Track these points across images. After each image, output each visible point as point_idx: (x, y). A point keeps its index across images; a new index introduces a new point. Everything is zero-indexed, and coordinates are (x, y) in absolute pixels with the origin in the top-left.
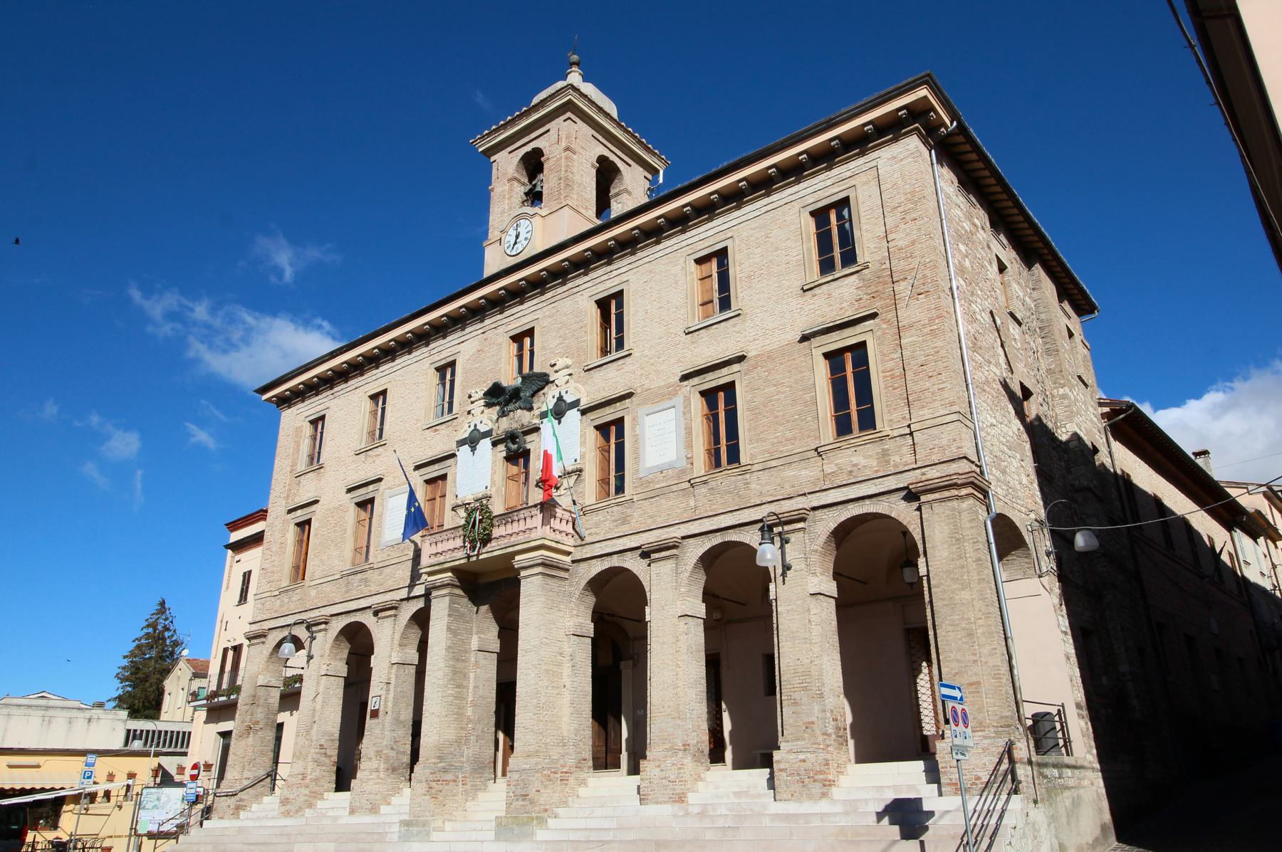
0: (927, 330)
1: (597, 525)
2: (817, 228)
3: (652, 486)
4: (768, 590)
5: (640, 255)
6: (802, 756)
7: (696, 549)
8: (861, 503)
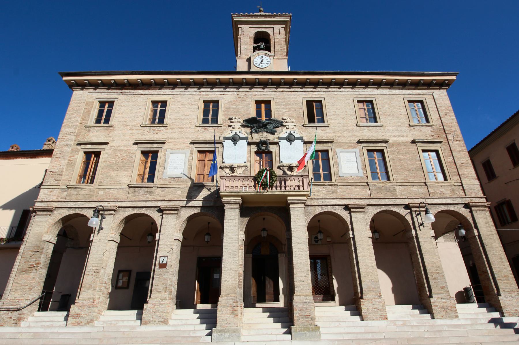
0: (462, 152)
1: (318, 192)
2: (100, 107)
3: (346, 181)
4: (90, 236)
5: (330, 90)
6: (444, 301)
7: (372, 212)
8: (446, 206)
